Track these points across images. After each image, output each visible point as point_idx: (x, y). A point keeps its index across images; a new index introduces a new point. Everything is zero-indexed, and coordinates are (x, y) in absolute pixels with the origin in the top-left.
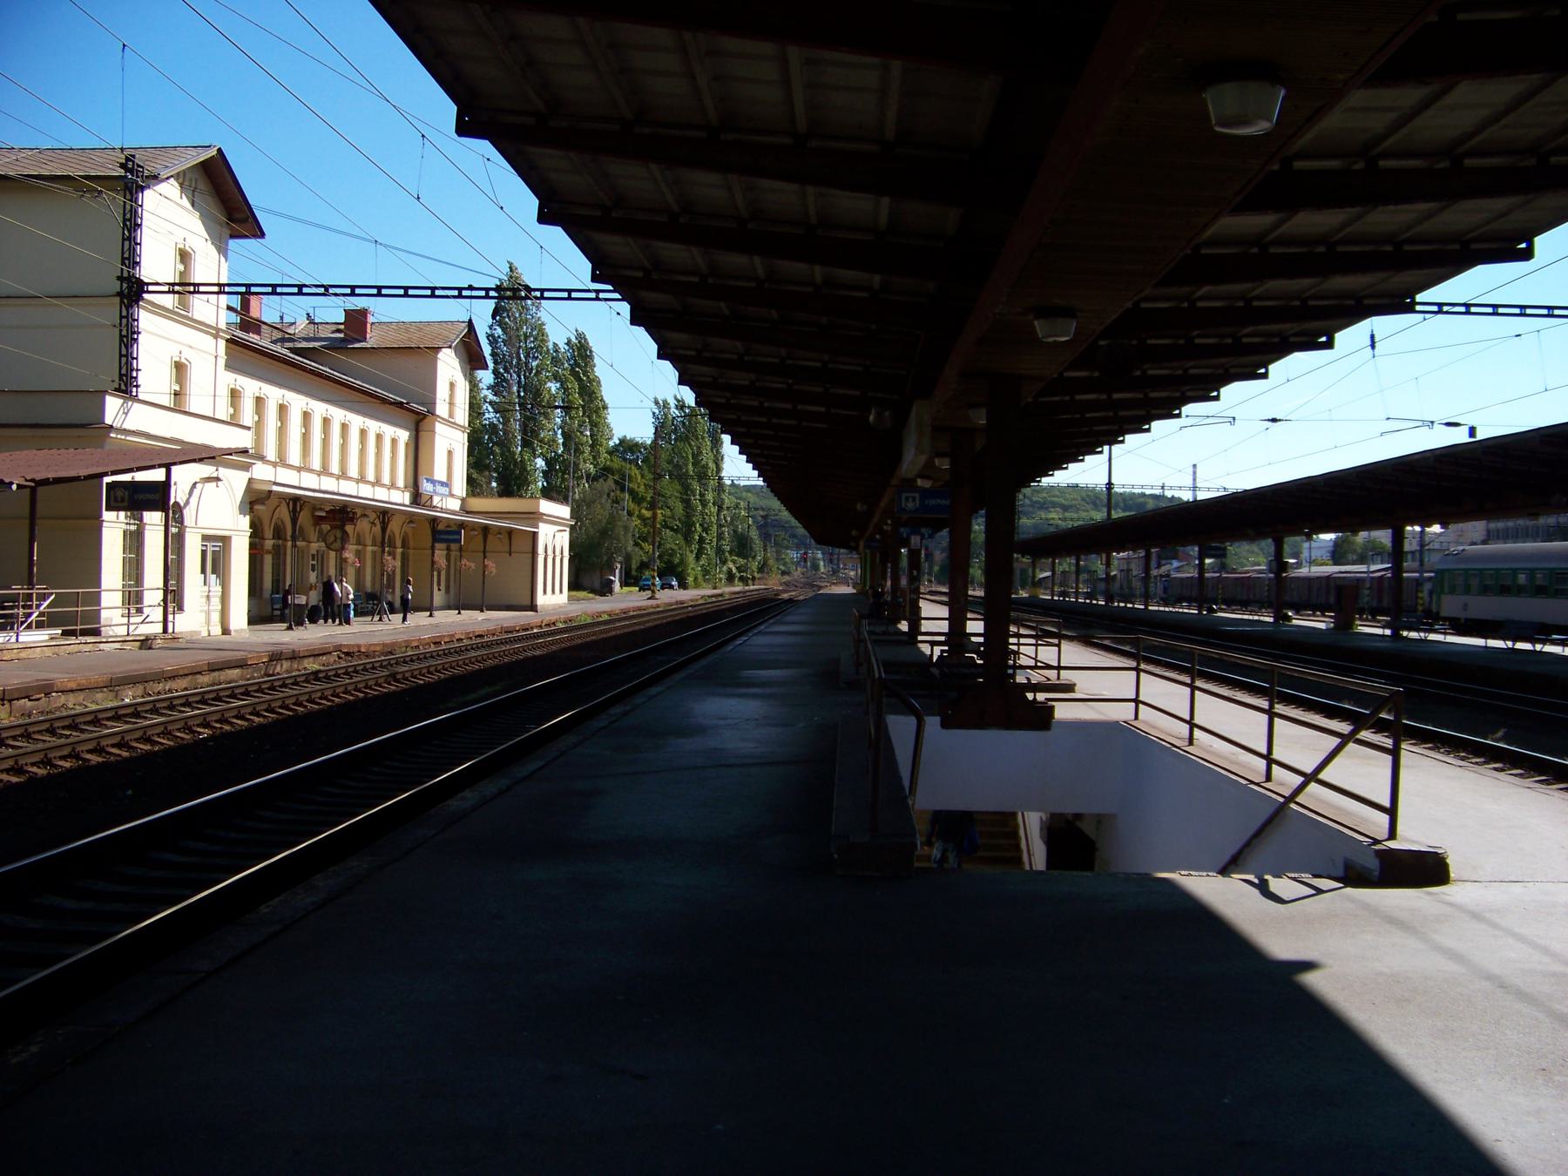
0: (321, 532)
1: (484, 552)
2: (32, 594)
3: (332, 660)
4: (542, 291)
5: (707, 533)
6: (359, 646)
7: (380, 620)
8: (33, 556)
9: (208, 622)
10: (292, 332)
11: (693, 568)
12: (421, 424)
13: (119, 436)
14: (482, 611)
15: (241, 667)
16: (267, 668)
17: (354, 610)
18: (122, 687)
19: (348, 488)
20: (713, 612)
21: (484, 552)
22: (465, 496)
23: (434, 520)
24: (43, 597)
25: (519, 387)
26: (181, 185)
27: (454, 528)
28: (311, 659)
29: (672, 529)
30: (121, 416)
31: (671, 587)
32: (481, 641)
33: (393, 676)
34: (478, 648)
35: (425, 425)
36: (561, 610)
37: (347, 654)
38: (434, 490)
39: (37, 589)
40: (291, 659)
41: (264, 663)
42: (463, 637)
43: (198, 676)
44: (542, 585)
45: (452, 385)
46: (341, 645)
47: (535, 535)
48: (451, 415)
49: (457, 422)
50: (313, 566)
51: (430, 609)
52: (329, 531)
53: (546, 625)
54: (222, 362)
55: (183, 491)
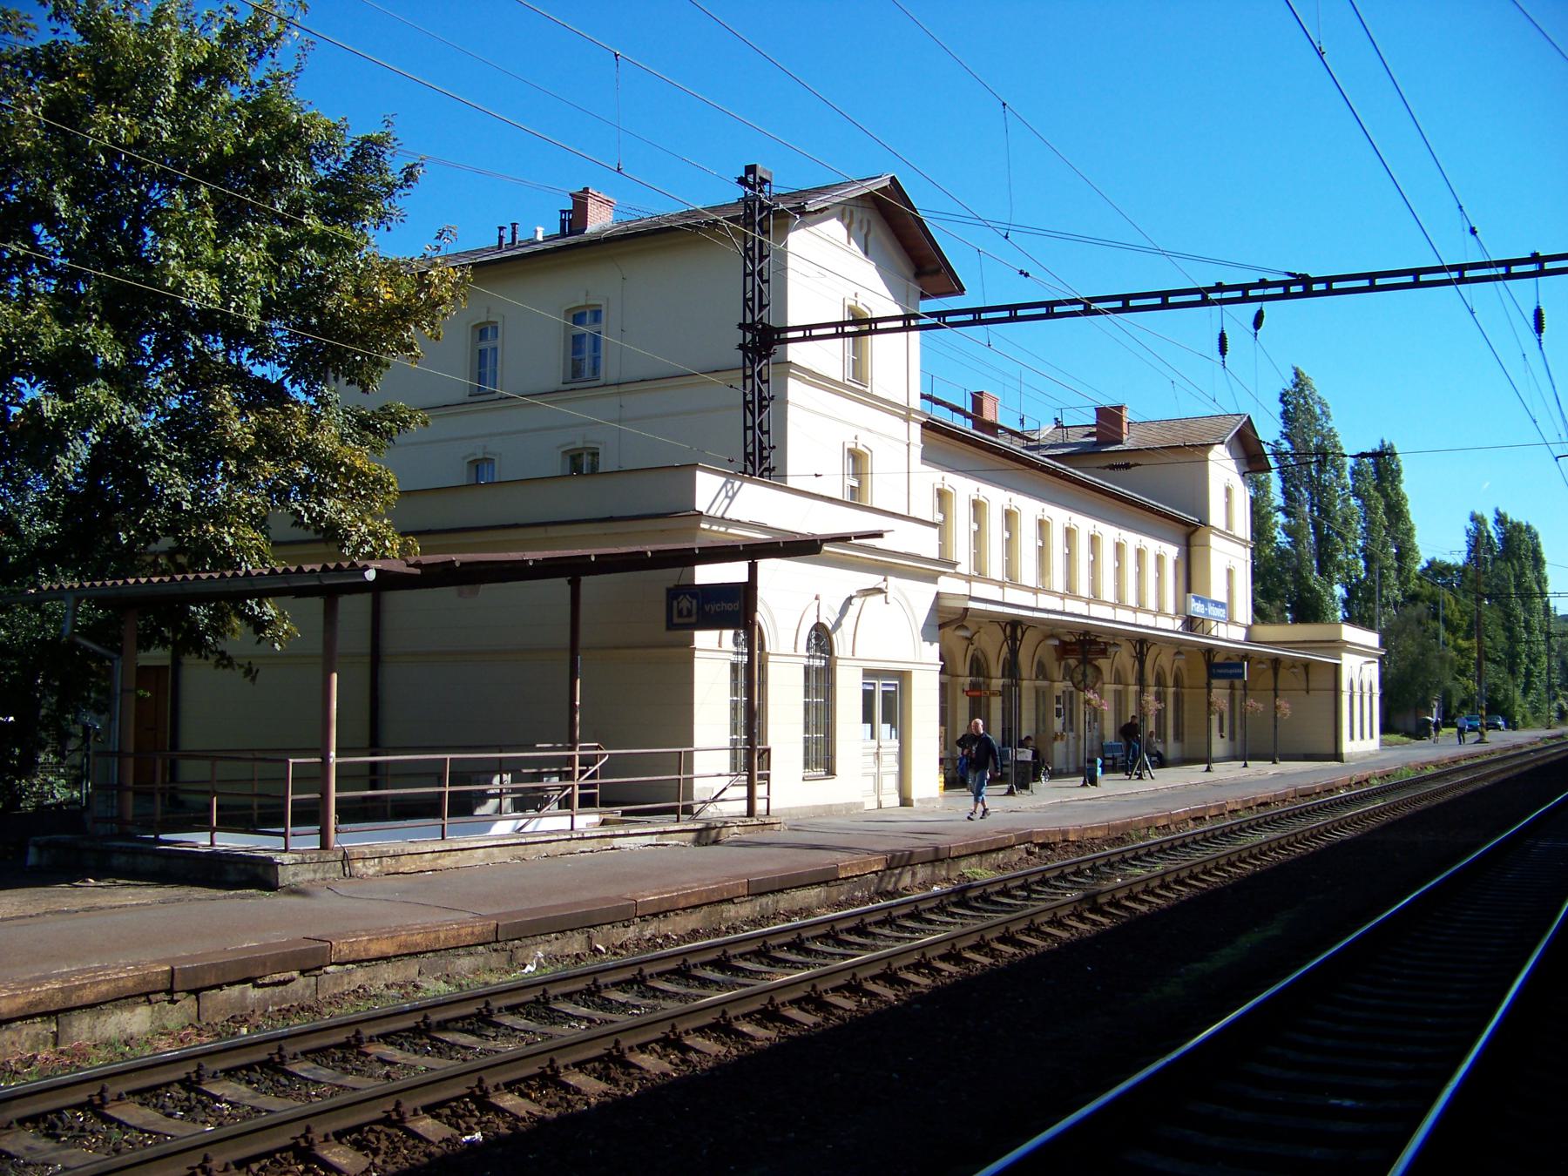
0: (1067, 667)
1: (1275, 690)
2: (574, 756)
3: (1016, 858)
4: (1328, 280)
5: (1535, 665)
6: (1065, 833)
7: (1140, 777)
8: (575, 700)
9: (878, 789)
10: (1037, 438)
11: (1521, 706)
12: (1192, 538)
13: (715, 528)
14: (1275, 762)
15: (826, 882)
16: (881, 880)
17: (1101, 766)
18: (528, 942)
19: (1102, 612)
20: (1559, 760)
21: (1275, 690)
22: (1250, 623)
23: (1209, 651)
24: (587, 761)
25: (1312, 505)
26: (848, 228)
27: (1236, 660)
28: (974, 860)
29: (1494, 661)
30: (722, 502)
31: (1497, 727)
32: (1266, 814)
33: (1091, 902)
34: (1259, 825)
35: (1196, 539)
36: (1372, 759)
37: (1043, 846)
38: (1206, 612)
39: (582, 749)
40: (932, 862)
41: (876, 872)
42: (1238, 807)
43: (724, 907)
44: (1348, 702)
45: (1228, 491)
46: (1031, 834)
47: (1337, 668)
48: (1229, 526)
49: (1237, 535)
50: (1058, 710)
51: (1207, 760)
52: (1077, 666)
53: (1356, 783)
54: (917, 451)
55: (829, 607)
